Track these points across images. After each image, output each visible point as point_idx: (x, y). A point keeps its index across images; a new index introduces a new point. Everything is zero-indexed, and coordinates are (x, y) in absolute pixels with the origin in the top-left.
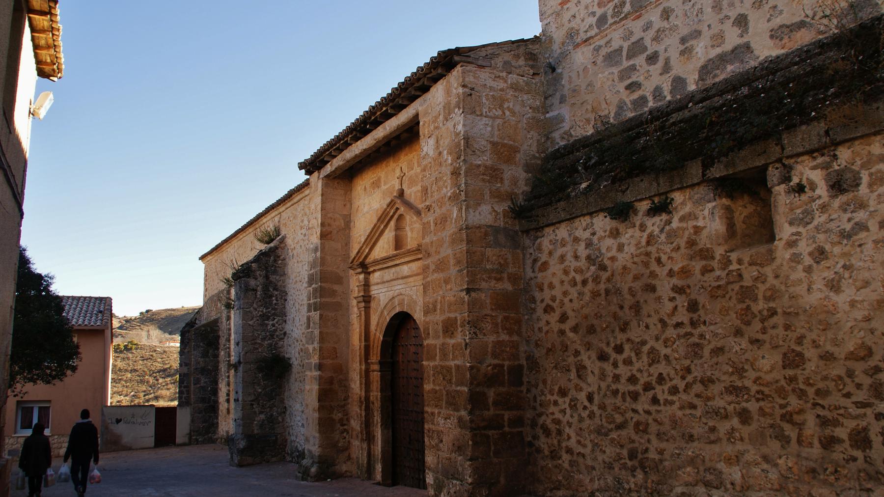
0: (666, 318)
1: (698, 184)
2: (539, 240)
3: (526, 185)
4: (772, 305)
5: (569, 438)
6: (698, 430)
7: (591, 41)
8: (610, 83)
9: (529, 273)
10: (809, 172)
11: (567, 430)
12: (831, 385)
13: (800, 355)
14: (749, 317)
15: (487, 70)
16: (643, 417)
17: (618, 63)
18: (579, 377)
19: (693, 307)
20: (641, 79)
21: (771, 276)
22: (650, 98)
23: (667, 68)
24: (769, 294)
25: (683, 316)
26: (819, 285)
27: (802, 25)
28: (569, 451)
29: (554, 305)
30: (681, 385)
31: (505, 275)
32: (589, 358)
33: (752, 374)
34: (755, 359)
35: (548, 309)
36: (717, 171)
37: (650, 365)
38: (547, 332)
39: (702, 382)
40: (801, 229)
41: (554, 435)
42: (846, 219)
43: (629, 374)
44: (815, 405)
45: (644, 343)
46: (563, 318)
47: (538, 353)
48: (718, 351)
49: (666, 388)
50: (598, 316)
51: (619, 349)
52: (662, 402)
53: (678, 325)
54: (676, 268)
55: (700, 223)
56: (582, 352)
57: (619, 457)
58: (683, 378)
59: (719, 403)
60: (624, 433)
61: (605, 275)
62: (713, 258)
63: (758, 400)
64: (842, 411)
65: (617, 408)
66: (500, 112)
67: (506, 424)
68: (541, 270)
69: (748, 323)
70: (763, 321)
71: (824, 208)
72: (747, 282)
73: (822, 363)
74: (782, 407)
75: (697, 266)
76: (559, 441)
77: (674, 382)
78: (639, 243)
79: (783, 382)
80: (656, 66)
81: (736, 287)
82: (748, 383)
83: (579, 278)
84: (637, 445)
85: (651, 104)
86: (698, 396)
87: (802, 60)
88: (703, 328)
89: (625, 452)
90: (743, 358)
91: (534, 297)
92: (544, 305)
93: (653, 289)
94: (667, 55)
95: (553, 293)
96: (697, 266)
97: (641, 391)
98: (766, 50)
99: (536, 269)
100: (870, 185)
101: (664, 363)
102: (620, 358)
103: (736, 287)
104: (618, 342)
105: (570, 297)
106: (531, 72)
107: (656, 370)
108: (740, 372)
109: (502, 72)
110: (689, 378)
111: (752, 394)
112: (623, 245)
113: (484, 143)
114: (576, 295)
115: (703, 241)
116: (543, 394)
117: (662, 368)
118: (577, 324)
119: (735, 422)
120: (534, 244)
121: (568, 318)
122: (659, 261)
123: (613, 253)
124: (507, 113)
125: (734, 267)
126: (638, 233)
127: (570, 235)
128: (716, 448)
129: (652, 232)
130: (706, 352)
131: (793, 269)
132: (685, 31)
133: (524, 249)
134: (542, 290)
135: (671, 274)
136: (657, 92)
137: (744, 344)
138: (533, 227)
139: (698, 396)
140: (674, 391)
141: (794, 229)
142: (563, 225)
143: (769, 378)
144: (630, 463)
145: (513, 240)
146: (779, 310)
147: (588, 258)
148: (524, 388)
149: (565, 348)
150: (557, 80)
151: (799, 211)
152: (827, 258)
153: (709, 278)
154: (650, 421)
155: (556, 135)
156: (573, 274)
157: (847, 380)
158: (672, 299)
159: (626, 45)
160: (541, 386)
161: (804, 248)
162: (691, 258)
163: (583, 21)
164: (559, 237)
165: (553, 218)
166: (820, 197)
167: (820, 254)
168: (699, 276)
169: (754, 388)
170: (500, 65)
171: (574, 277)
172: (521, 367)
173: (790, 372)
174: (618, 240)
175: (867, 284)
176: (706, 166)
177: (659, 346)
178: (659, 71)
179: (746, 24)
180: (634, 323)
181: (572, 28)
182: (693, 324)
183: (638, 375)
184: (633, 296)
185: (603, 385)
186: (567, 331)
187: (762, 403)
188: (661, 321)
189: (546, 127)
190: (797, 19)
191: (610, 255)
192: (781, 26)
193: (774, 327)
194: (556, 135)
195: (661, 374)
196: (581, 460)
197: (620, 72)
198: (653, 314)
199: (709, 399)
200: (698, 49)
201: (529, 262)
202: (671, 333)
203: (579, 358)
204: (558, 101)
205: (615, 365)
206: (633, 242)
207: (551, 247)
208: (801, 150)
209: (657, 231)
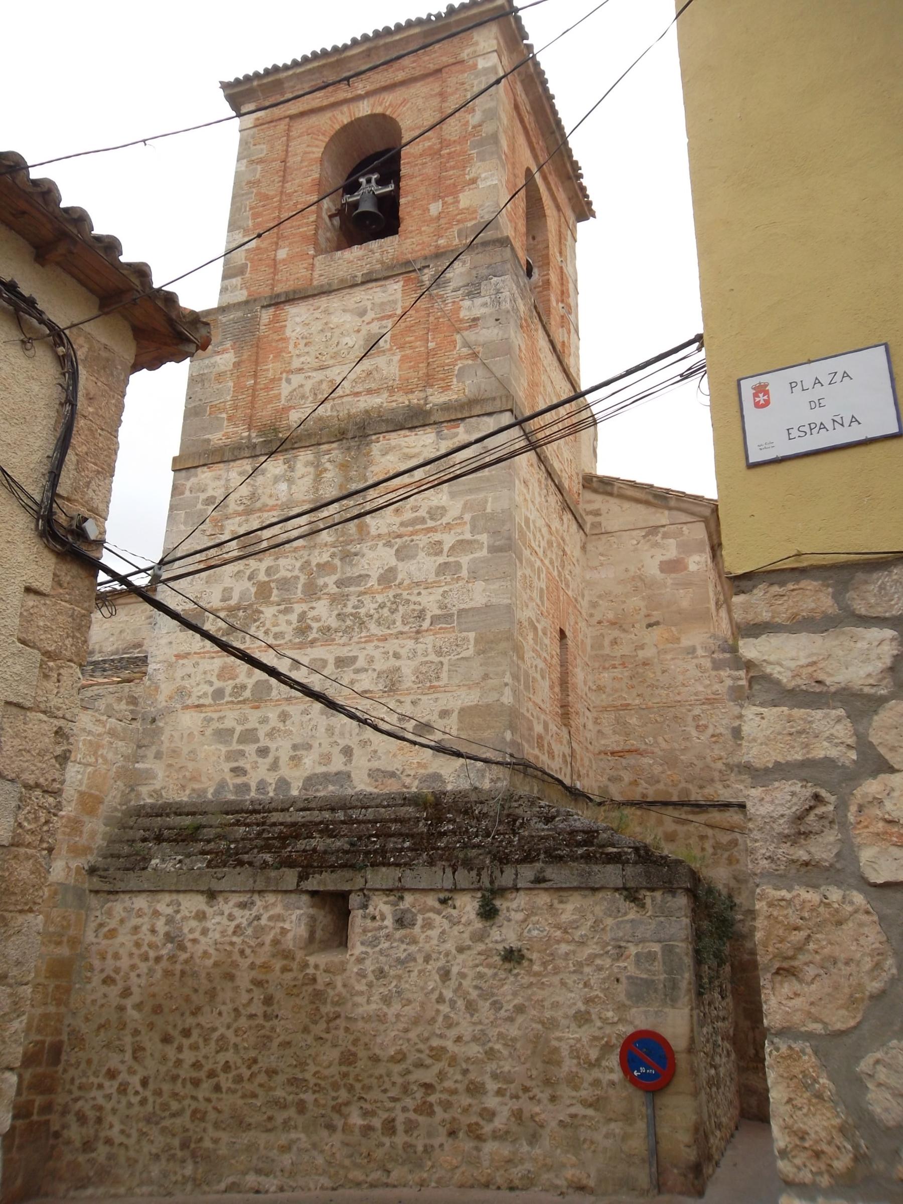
0: (241, 1008)
1: (291, 892)
2: (109, 904)
3: (103, 839)
4: (337, 1009)
5: (111, 1126)
6: (257, 1118)
7: (204, 709)
8: (215, 758)
9: (90, 937)
10: (381, 905)
11: (110, 1118)
12: (374, 1081)
13: (354, 1055)
14: (317, 1017)
15: (90, 712)
16: (202, 1105)
17: (227, 742)
18: (135, 1058)
19: (268, 1001)
20: (248, 767)
21: (339, 984)
22: (253, 788)
23: (274, 766)
24: (336, 999)
25: (257, 1008)
26: (375, 998)
27: (393, 775)
28: (109, 1142)
29: (117, 977)
30: (246, 1073)
31: (65, 939)
32: (150, 1040)
33: (312, 1068)
34: (317, 1055)
35: (108, 981)
36: (312, 884)
37: (217, 1052)
38: (102, 1006)
39: (267, 1072)
40: (369, 950)
41: (91, 1123)
42: (402, 949)
43: (193, 1060)
44: (361, 1098)
45: (214, 1029)
46: (126, 993)
47: (85, 1028)
48: (286, 1044)
49: (230, 1076)
50: (169, 996)
51: (186, 1033)
52: (224, 1090)
53: (252, 1016)
54: (258, 962)
55: (287, 926)
56: (143, 1032)
57: (168, 1148)
58: (249, 1067)
59: (279, 1093)
60: (178, 1121)
61: (183, 956)
62: (294, 959)
63: (314, 1092)
64: (379, 1105)
65: (175, 1095)
66: (93, 760)
67: (35, 1111)
68: (106, 937)
69: (315, 1022)
70: (328, 1022)
71: (388, 937)
72: (320, 986)
73: (370, 1063)
74: (334, 1099)
75: (278, 964)
76: (97, 1131)
77: (240, 1071)
78: (225, 931)
79: (337, 1078)
80: (265, 760)
81: (310, 989)
82: (308, 1076)
83: (152, 954)
84: (190, 1133)
85: (253, 794)
86: (261, 1085)
87: (388, 806)
88: (275, 1022)
89: (176, 1142)
90: (307, 1053)
91: (91, 965)
92: (104, 975)
93: (231, 977)
94: (278, 754)
95: (118, 964)
96: (278, 964)
97: (204, 1078)
98: (362, 784)
99: (101, 935)
100: (423, 927)
101: (232, 1051)
102: (186, 1042)
103: (310, 989)
104: (187, 1026)
105: (138, 971)
106: (130, 717)
107: (222, 1058)
108: (302, 1065)
109: (103, 714)
110: (255, 1068)
111: (311, 1085)
112: (208, 930)
113: (72, 792)
114: (146, 970)
115: (289, 942)
116: (84, 1073)
117: (229, 1056)
118: (142, 1002)
119: (292, 1112)
120: (102, 907)
121: (131, 994)
122: (242, 952)
123: (196, 935)
124: (100, 761)
125: (311, 971)
126: (225, 921)
127: (150, 907)
128: (271, 1136)
129: (241, 923)
130: (276, 1042)
131: (358, 981)
132: (298, 740)
133: (89, 909)
134: (104, 958)
135: (252, 966)
136: (262, 786)
137: (310, 1039)
138: (106, 888)
139: (261, 1085)
140: (239, 1079)
141: (364, 949)
142: (144, 895)
143: (326, 1072)
144: (180, 1154)
145: (80, 895)
146: (343, 1015)
147: (167, 934)
148: (60, 1068)
149: (123, 1026)
150: (158, 732)
151: (370, 934)
152: (384, 977)
153: (288, 976)
154: (210, 1108)
155: (144, 790)
156: (145, 948)
157: (386, 1079)
158: (249, 991)
159: (239, 729)
160: (83, 1066)
161: (369, 966)
162: (274, 956)
163: (198, 684)
164: (137, 906)
165: (132, 885)
166: (386, 927)
167: (381, 973)
168: (278, 973)
169: (312, 1081)
170: (103, 707)
171: (146, 952)
172: (61, 1043)
173: (344, 1069)
174: (204, 924)
175: (409, 1002)
176: (302, 877)
177: (230, 1034)
178: (267, 767)
179: (351, 756)
180: (207, 1009)
181: (184, 688)
182: (266, 1016)
183: (203, 1062)
184: (210, 981)
185: (163, 1069)
186: (129, 1007)
187: (317, 1096)
188: (236, 1010)
189: (133, 779)
190: (390, 769)
191: (191, 936)
192: (378, 770)
193: (336, 1029)
194: (144, 790)
195: (227, 1062)
196: (122, 1152)
197: (228, 752)
198: (228, 1001)
199: (271, 1089)
200: (306, 760)
201: (92, 925)
202: (243, 1022)
203: (138, 1038)
204: (152, 756)
205: (180, 1049)
206: (219, 928)
207: (123, 914)
208: (378, 886)
209: (245, 923)
